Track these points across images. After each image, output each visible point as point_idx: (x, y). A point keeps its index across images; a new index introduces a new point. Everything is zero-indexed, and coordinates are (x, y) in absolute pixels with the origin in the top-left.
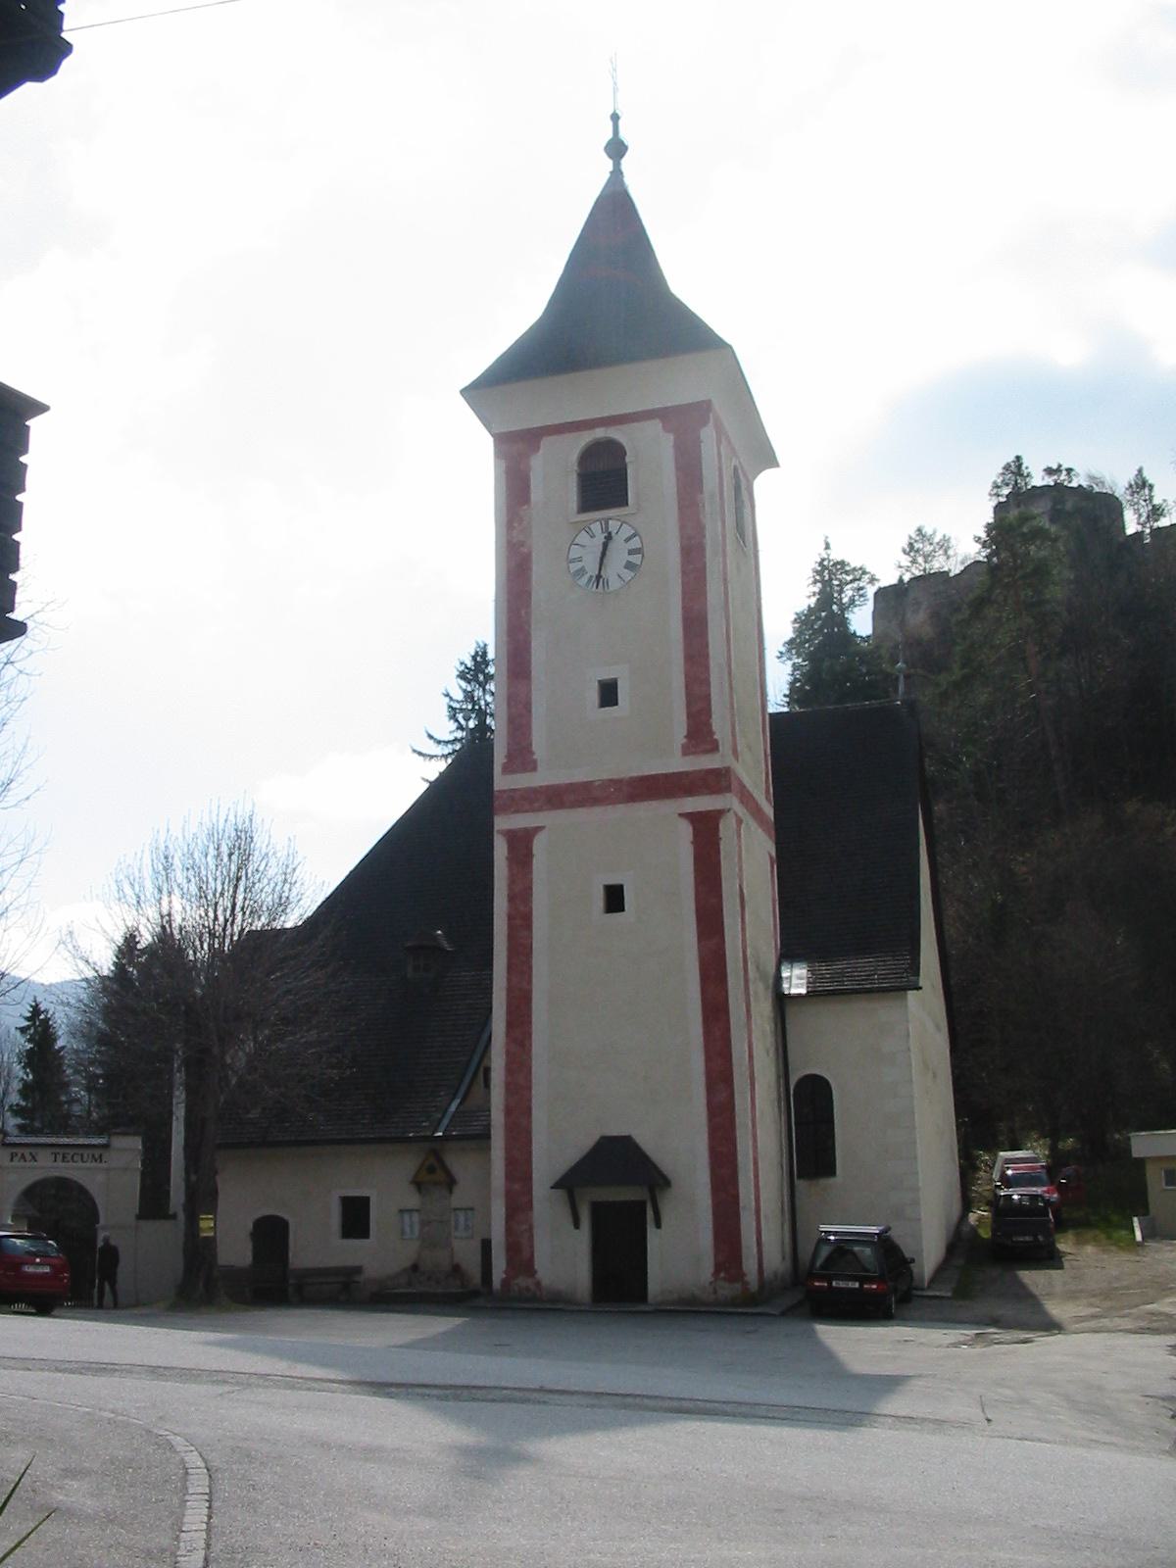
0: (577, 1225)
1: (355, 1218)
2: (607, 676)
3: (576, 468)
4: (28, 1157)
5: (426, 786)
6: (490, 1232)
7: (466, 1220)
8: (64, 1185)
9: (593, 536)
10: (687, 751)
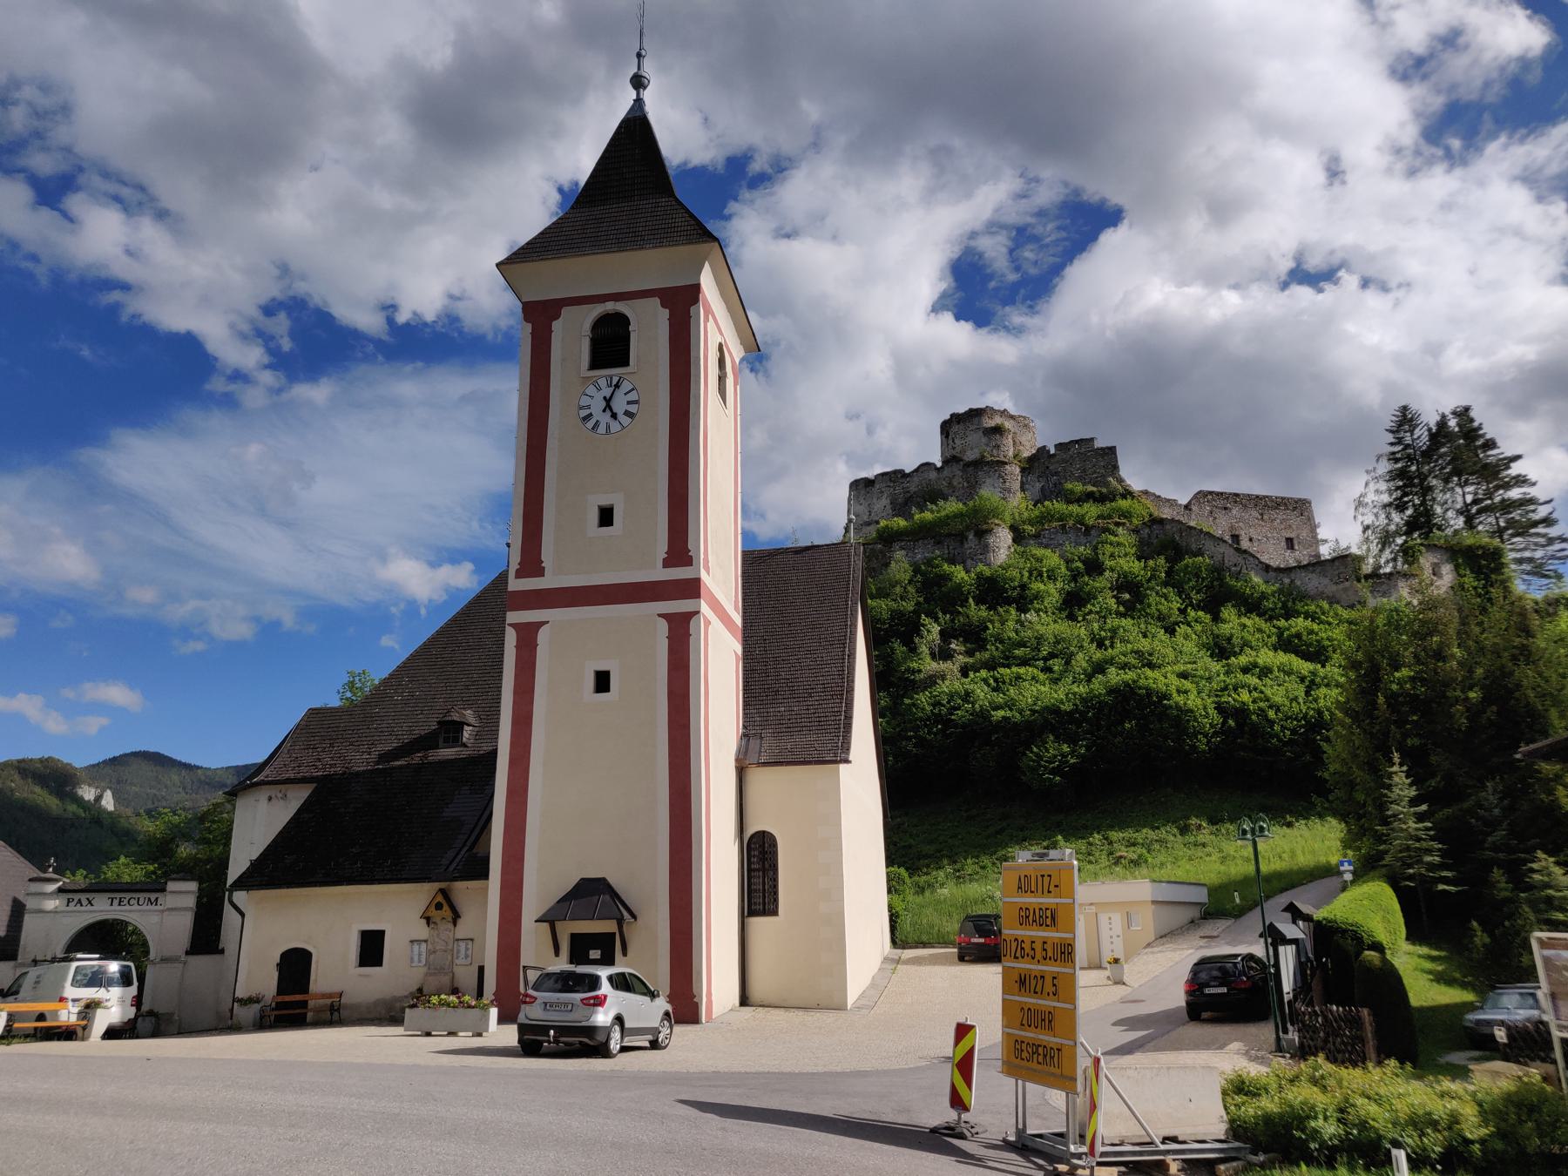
0: (557, 953)
1: (372, 948)
2: (605, 502)
3: (589, 333)
4: (85, 902)
5: (1001, 975)
6: (484, 962)
7: (467, 949)
8: (436, 905)
9: (599, 389)
10: (667, 563)
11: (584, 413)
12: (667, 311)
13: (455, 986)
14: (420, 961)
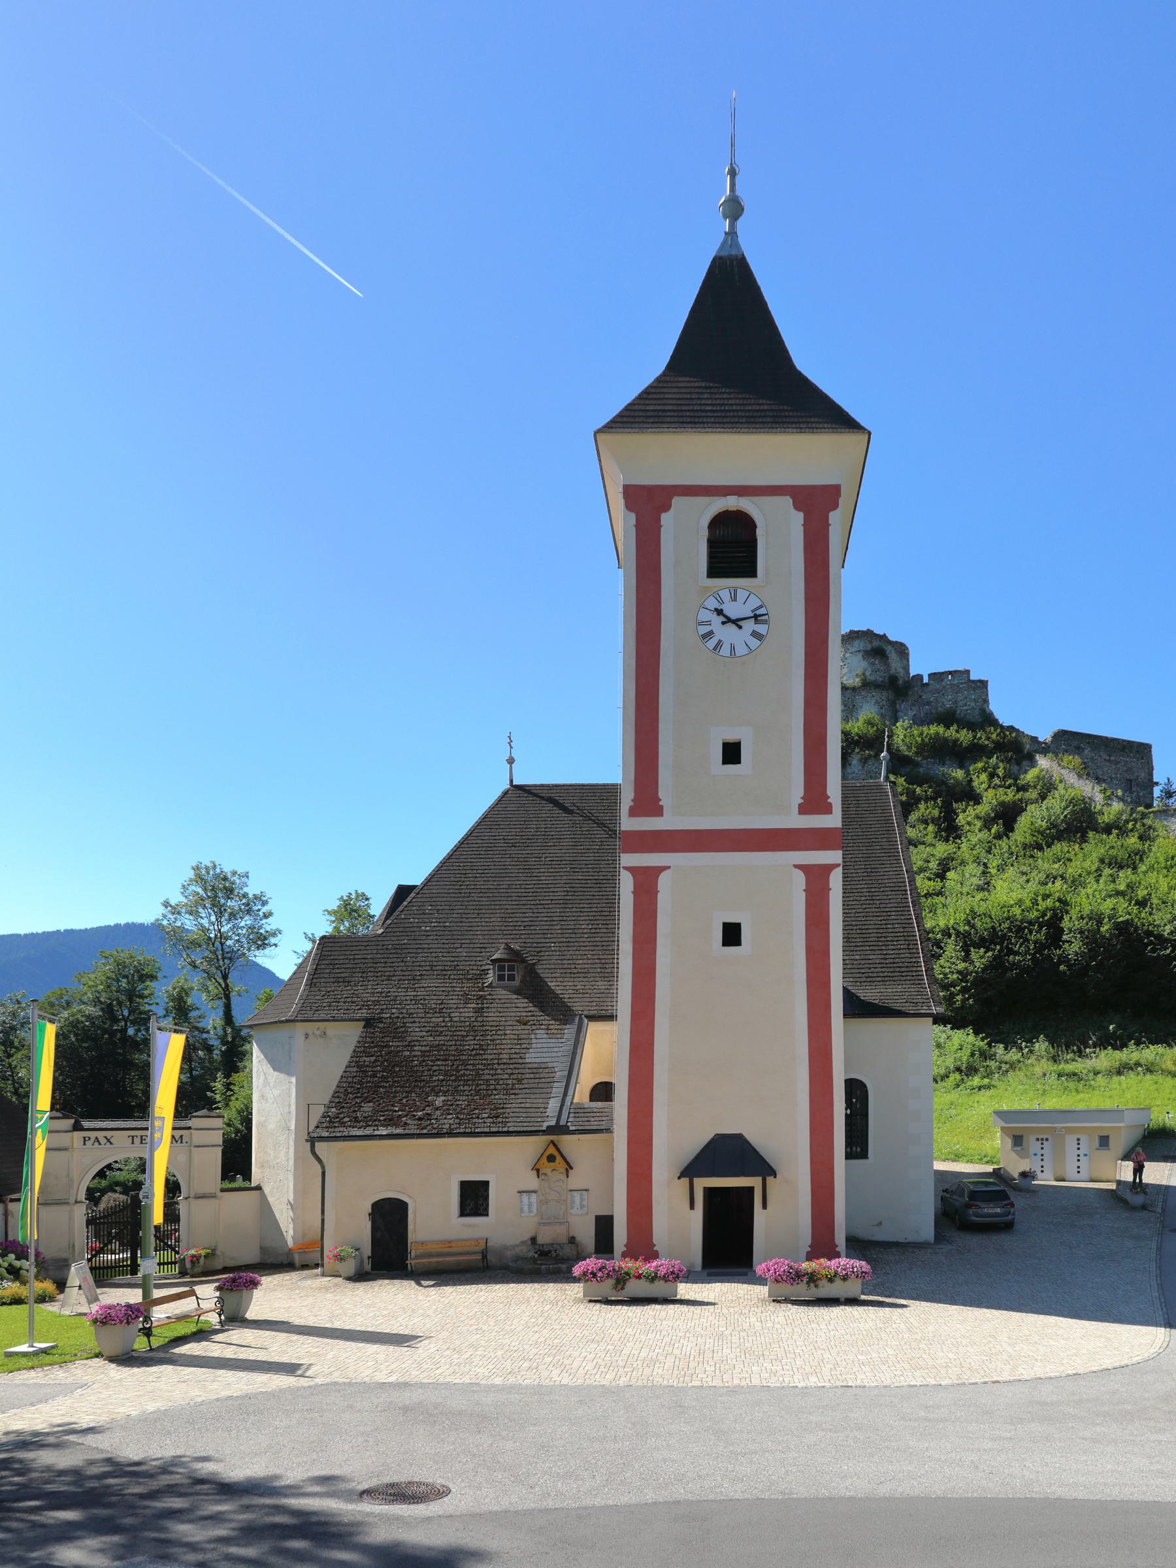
0: (692, 1207)
2: (731, 737)
4: (103, 1141)
7: (582, 1200)
10: (804, 809)
11: (703, 630)
12: (801, 515)
13: (571, 1235)
14: (530, 1211)
